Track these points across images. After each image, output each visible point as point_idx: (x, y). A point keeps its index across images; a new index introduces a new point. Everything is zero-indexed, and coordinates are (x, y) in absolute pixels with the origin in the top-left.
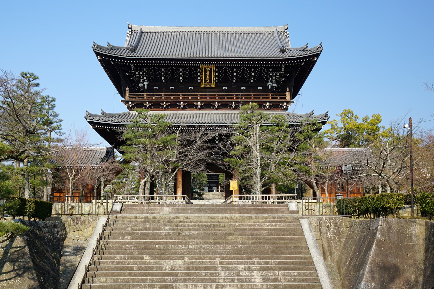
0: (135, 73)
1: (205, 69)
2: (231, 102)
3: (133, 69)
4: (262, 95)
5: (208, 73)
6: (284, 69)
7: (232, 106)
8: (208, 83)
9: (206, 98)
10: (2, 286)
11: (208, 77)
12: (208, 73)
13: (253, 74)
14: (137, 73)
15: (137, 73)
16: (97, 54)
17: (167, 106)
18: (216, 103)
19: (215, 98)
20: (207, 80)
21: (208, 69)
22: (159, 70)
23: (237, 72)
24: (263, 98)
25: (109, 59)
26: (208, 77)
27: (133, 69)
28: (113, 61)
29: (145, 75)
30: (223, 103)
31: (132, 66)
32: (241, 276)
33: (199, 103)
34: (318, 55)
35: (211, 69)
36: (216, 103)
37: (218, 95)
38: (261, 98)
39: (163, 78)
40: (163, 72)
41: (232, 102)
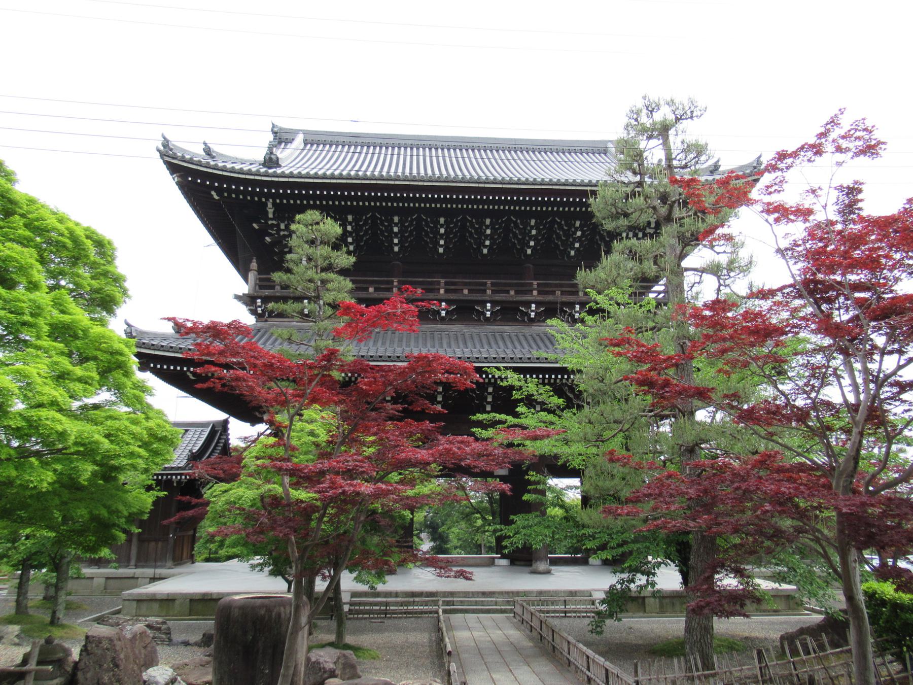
0: (278, 226)
2: (528, 304)
3: (271, 216)
4: (561, 286)
6: (274, 213)
7: (439, 313)
10: (900, 658)
13: (488, 232)
14: (282, 226)
15: (282, 226)
16: (173, 168)
19: (484, 291)
23: (403, 225)
24: (563, 293)
25: (203, 183)
27: (271, 216)
28: (216, 189)
29: (531, 239)
31: (270, 205)
41: (530, 303)
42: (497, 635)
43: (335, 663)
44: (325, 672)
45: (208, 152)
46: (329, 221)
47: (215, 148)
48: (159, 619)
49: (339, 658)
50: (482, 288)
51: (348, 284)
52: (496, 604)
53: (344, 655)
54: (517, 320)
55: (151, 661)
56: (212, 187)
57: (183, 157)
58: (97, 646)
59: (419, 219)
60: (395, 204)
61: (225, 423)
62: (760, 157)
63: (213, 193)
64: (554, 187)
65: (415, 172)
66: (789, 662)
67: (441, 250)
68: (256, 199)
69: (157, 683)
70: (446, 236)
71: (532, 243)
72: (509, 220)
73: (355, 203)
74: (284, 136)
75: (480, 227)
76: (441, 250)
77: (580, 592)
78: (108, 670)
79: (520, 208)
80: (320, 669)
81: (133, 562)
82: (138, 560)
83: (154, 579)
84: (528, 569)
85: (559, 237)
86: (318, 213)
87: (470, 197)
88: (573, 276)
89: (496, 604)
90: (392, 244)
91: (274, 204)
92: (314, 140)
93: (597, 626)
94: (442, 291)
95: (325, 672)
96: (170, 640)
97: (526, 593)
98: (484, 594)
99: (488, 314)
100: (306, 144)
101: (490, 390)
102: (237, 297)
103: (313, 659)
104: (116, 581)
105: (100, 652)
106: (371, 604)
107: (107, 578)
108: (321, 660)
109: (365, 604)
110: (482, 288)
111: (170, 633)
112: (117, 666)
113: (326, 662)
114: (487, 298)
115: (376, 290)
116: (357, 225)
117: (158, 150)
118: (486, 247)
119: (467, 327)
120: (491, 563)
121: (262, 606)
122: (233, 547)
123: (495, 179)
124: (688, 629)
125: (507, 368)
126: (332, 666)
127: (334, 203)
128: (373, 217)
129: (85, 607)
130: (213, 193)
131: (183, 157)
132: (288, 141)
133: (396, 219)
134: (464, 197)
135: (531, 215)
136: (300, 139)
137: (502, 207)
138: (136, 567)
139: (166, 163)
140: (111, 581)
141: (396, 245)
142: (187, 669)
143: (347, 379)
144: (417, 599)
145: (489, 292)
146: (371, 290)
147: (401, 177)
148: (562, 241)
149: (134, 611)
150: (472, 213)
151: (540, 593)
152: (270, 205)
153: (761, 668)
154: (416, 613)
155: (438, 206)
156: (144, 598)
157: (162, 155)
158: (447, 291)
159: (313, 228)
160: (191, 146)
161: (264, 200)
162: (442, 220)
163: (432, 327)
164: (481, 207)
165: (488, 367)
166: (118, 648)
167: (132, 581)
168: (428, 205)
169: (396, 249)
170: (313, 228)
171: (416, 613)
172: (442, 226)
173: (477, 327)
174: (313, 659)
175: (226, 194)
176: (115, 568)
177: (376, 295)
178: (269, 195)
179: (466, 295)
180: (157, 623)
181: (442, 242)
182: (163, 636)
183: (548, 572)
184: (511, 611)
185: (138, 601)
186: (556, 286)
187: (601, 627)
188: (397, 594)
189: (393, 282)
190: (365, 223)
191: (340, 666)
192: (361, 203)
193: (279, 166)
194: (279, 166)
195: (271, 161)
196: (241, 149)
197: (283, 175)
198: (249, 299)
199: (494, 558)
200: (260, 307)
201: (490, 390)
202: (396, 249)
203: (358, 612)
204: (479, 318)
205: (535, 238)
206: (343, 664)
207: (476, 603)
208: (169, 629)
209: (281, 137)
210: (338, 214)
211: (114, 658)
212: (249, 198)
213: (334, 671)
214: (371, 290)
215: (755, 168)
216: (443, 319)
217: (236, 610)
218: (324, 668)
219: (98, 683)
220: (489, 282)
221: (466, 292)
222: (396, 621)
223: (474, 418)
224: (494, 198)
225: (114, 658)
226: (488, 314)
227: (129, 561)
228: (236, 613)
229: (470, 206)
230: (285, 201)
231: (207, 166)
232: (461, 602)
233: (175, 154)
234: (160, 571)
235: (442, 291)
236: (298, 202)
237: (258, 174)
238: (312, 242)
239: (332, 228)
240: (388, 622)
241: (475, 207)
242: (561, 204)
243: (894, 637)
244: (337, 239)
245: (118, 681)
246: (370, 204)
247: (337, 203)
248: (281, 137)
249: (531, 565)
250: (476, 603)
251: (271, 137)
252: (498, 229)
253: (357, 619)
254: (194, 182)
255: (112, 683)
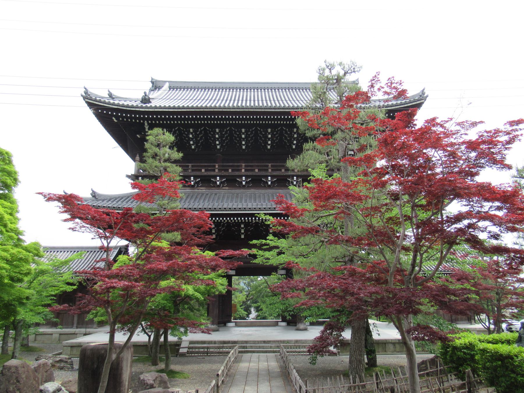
2: (266, 177)
7: (267, 183)
16: (90, 105)
17: (221, 183)
18: (244, 178)
19: (267, 170)
22: (212, 131)
28: (115, 116)
29: (294, 140)
31: (146, 124)
34: (419, 106)
36: (244, 178)
39: (217, 143)
40: (218, 133)
41: (267, 176)
42: (263, 365)
43: (154, 380)
44: (148, 385)
45: (111, 95)
46: (167, 134)
47: (115, 93)
48: (67, 357)
49: (157, 378)
50: (266, 168)
51: (179, 169)
52: (271, 347)
53: (160, 376)
54: (262, 186)
55: (50, 379)
56: (112, 115)
57: (96, 99)
58: (8, 371)
59: (256, 130)
60: (199, 122)
61: (127, 246)
62: (424, 89)
63: (114, 118)
64: (245, 110)
65: (257, 104)
66: (393, 379)
67: (269, 147)
68: (138, 121)
69: (48, 391)
70: (272, 139)
71: (295, 142)
72: (282, 129)
73: (206, 122)
74: (158, 84)
75: (291, 134)
76: (269, 147)
77: (299, 341)
78: (13, 384)
79: (286, 122)
80: (145, 384)
81: (75, 325)
82: (78, 323)
83: (85, 334)
84: (295, 328)
85: (286, 137)
86: (161, 129)
87: (263, 117)
88: (285, 162)
89: (271, 347)
90: (241, 145)
91: (148, 124)
92: (175, 87)
93: (313, 360)
94: (243, 170)
95: (148, 385)
96: (72, 368)
97: (288, 342)
98: (264, 342)
99: (269, 183)
100: (170, 89)
101: (242, 226)
102: (128, 176)
103: (142, 378)
104: (66, 336)
105: (9, 374)
106: (199, 348)
107: (60, 334)
108: (146, 379)
109: (196, 348)
110: (266, 168)
111: (72, 364)
112: (18, 381)
113: (149, 380)
114: (269, 174)
115: (206, 170)
116: (221, 134)
117: (82, 96)
118: (294, 144)
119: (257, 190)
120: (276, 324)
121: (102, 349)
122: (102, 317)
123: (298, 106)
124: (351, 362)
125: (265, 214)
126: (152, 382)
127: (188, 122)
128: (231, 130)
129: (45, 350)
130: (114, 118)
131: (96, 99)
132: (160, 88)
133: (243, 130)
134: (260, 117)
135: (269, 126)
136: (167, 85)
137: (276, 122)
138: (77, 328)
139: (87, 102)
140: (63, 336)
141: (244, 145)
142: (70, 384)
143: (219, 221)
144: (225, 345)
145: (270, 170)
146: (203, 170)
147: (240, 107)
148: (288, 140)
149: (69, 352)
150: (235, 125)
151: (297, 341)
152: (146, 124)
153: (377, 383)
154: (224, 353)
155: (246, 122)
156: (75, 345)
157: (84, 98)
158: (246, 170)
159: (160, 137)
160: (100, 92)
161: (142, 121)
162: (269, 130)
163: (263, 191)
164: (288, 122)
165: (258, 214)
166: (20, 372)
167: (75, 336)
168: (234, 122)
169: (244, 147)
170: (160, 137)
171: (224, 353)
172: (269, 133)
173: (263, 190)
174: (142, 378)
175: (121, 119)
176: (61, 328)
177: (206, 174)
178: (144, 119)
179: (257, 173)
180: (66, 358)
181: (269, 142)
182: (69, 366)
183: (306, 329)
184: (279, 352)
185: (72, 347)
186: (229, 166)
187: (315, 360)
188: (215, 342)
189: (215, 166)
190: (226, 133)
191: (158, 382)
192: (209, 122)
193: (150, 102)
194: (150, 102)
195: (146, 100)
196: (129, 92)
197: (151, 107)
198: (134, 177)
199: (278, 322)
200: (193, 181)
201: (242, 226)
202: (244, 147)
203: (192, 353)
204: (266, 186)
205: (190, 139)
206: (160, 381)
207: (260, 347)
208: (72, 362)
209: (156, 86)
210: (169, 128)
211: (17, 377)
212: (134, 121)
213: (153, 385)
214: (203, 170)
215: (421, 96)
216: (269, 186)
217: (89, 351)
218: (147, 383)
219: (7, 391)
220: (270, 165)
221: (257, 170)
222: (212, 358)
223: (251, 242)
224: (277, 117)
225: (17, 377)
226: (269, 183)
227: (73, 324)
228: (89, 352)
229: (261, 122)
230: (154, 122)
231: (109, 103)
232: (251, 346)
233: (91, 97)
234: (88, 330)
235: (243, 170)
236: (172, 122)
237: (137, 107)
238: (158, 146)
239: (170, 137)
240: (207, 358)
241: (261, 122)
242: (207, 119)
243: (454, 365)
244: (171, 143)
245: (19, 390)
246: (214, 122)
247: (186, 122)
248: (156, 86)
249: (296, 326)
250: (260, 347)
251: (151, 85)
252: (276, 134)
253: (191, 356)
254: (102, 112)
255: (14, 391)
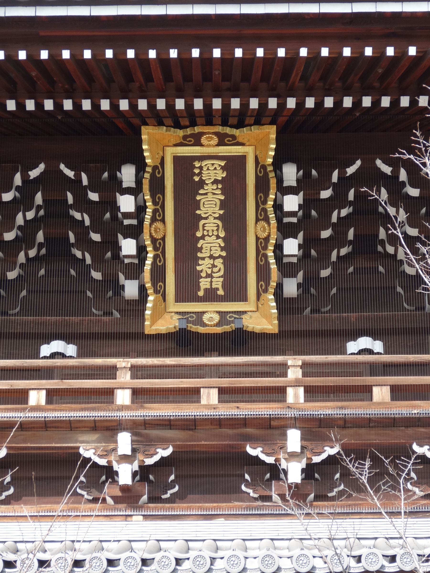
1: (184, 165)
5: (210, 204)
8: (211, 296)
9: (193, 394)
11: (211, 243)
12: (210, 204)
18: (294, 439)
20: (204, 266)
21: (212, 172)
24: (398, 393)
26: (211, 243)
30: (353, 437)
32: (206, 325)
33: (124, 442)
35: (235, 165)
37: (306, 368)
38: (381, 393)
